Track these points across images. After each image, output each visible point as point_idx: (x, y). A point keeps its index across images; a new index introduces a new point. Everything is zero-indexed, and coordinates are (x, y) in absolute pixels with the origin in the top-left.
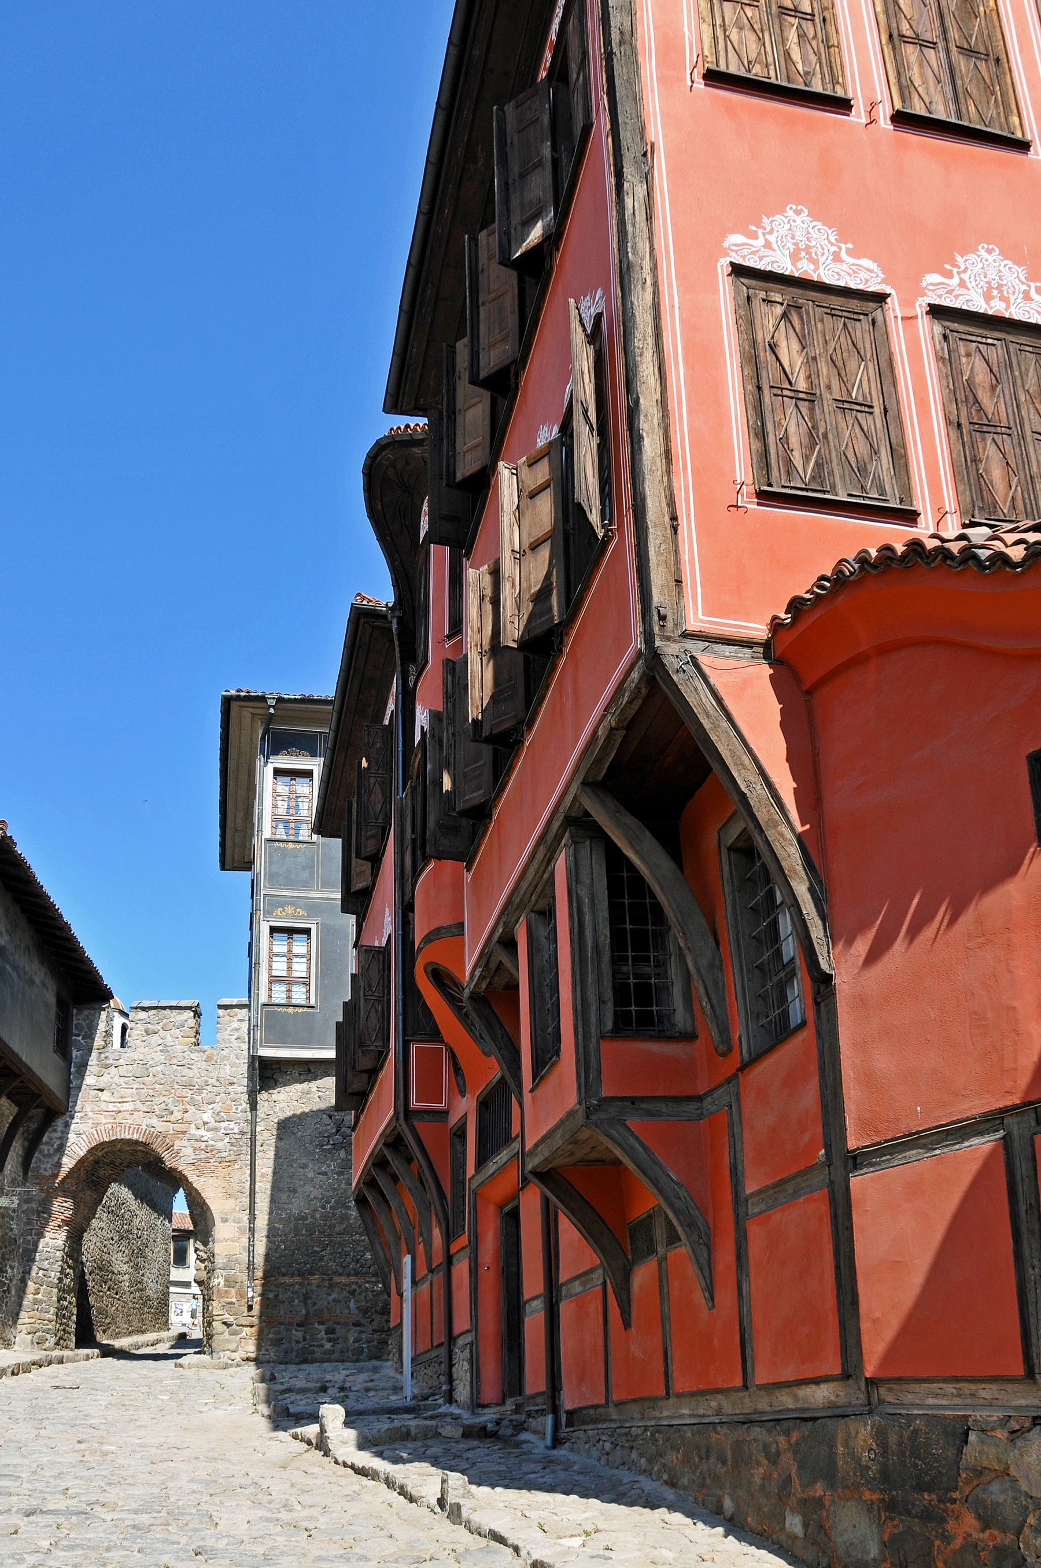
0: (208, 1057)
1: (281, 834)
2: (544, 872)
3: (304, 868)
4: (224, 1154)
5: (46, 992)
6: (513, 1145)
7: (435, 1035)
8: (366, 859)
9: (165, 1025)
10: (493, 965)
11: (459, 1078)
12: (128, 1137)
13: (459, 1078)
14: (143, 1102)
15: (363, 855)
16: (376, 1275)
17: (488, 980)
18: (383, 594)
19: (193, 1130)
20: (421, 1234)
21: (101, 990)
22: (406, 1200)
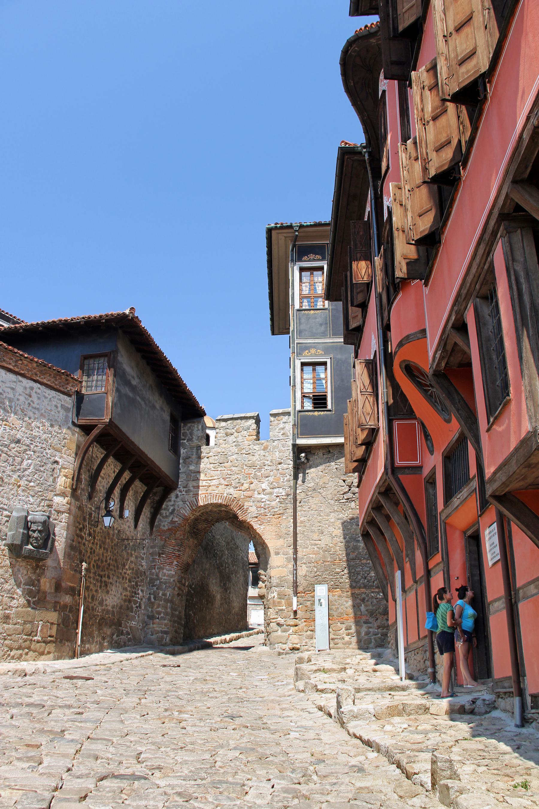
0: (264, 447)
1: (306, 305)
2: (485, 264)
3: (321, 325)
4: (276, 510)
5: (160, 410)
6: (471, 484)
7: (410, 414)
8: (357, 306)
9: (237, 429)
10: (449, 348)
11: (429, 442)
12: (215, 502)
13: (429, 442)
15: (355, 304)
16: (377, 587)
17: (446, 360)
18: (357, 137)
19: (256, 495)
20: (407, 556)
21: (198, 410)
22: (397, 533)
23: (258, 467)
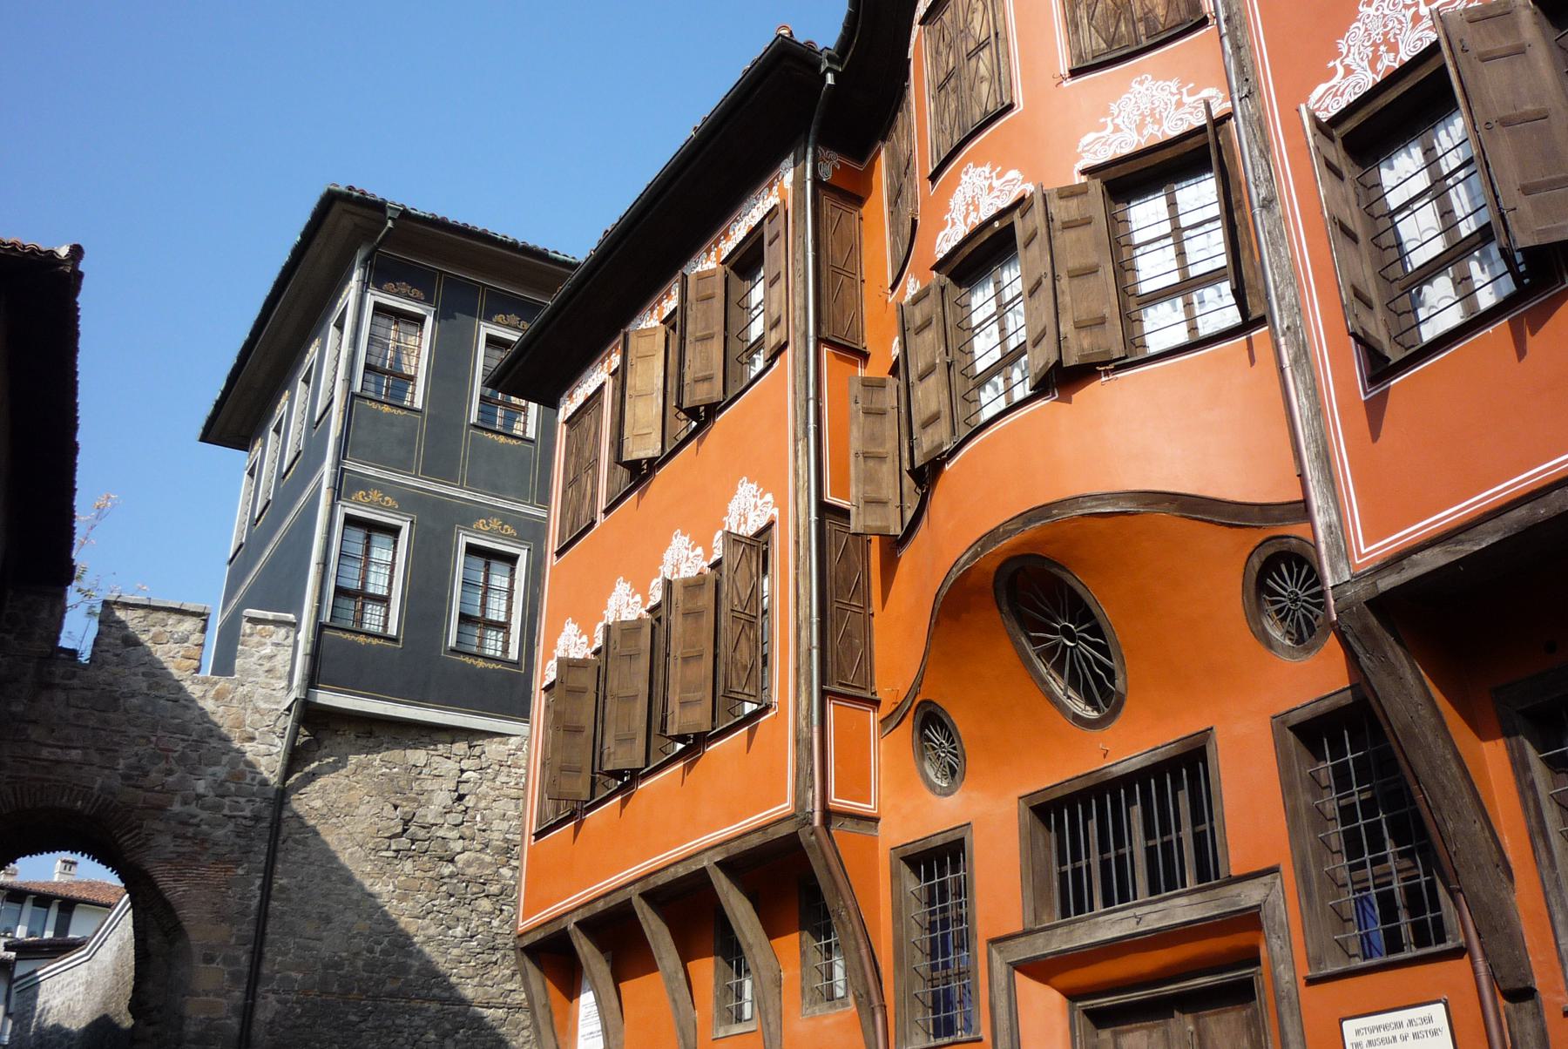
23: (195, 737)
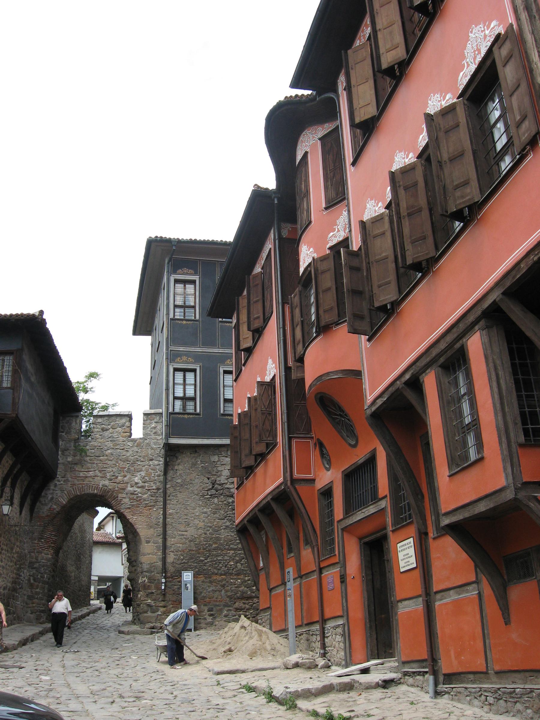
9: (113, 425)
14: (100, 471)
